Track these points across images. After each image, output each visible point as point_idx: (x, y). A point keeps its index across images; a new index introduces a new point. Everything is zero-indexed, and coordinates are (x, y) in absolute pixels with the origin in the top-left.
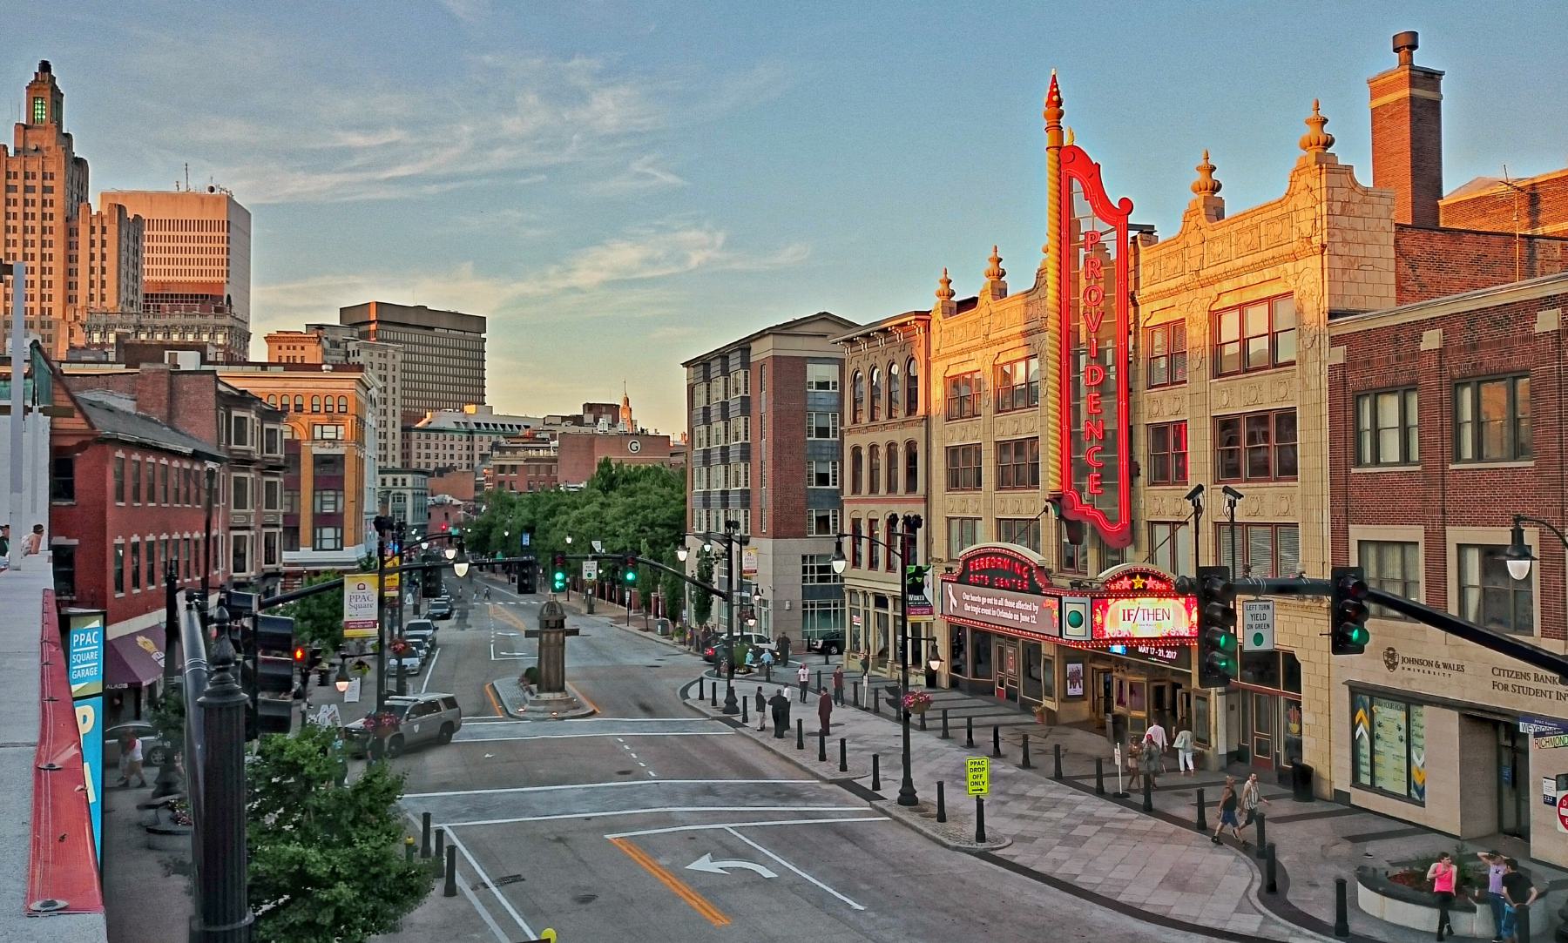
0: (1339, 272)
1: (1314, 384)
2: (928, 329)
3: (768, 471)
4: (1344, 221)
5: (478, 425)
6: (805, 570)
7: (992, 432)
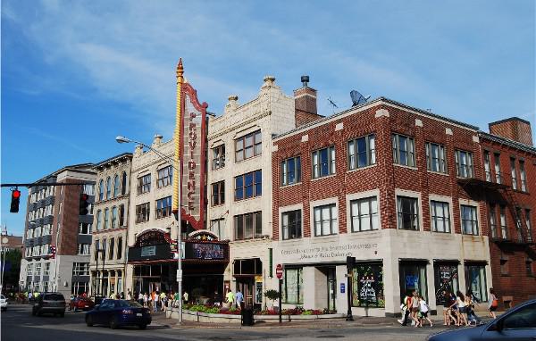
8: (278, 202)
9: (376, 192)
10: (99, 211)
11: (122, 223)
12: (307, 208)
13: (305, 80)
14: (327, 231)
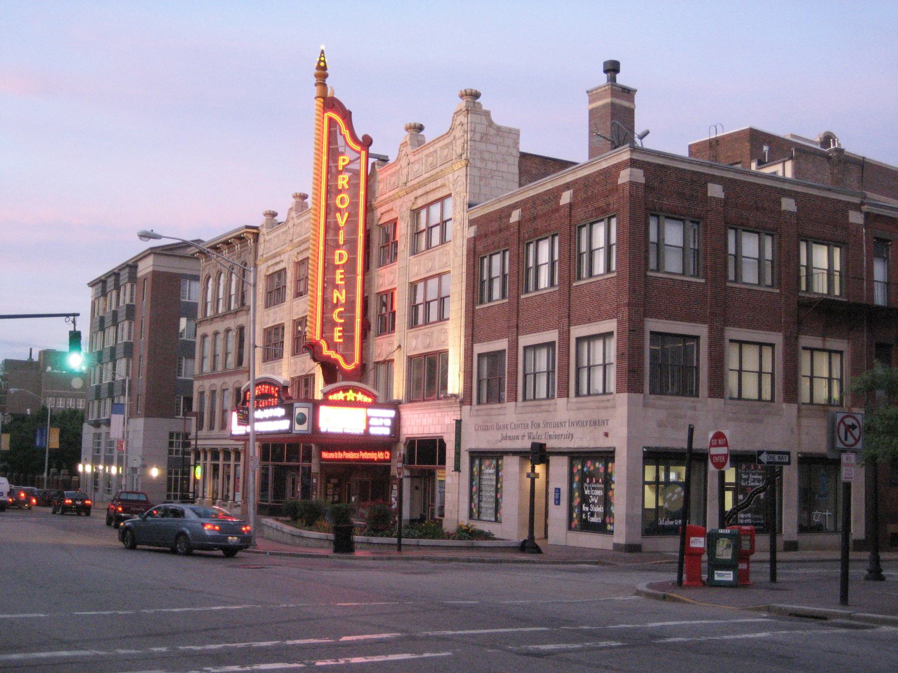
0: (477, 179)
3: (145, 362)
4: (482, 146)
6: (171, 444)
8: (472, 335)
9: (610, 325)
10: (204, 336)
11: (240, 361)
12: (514, 345)
13: (612, 68)
14: (598, 386)
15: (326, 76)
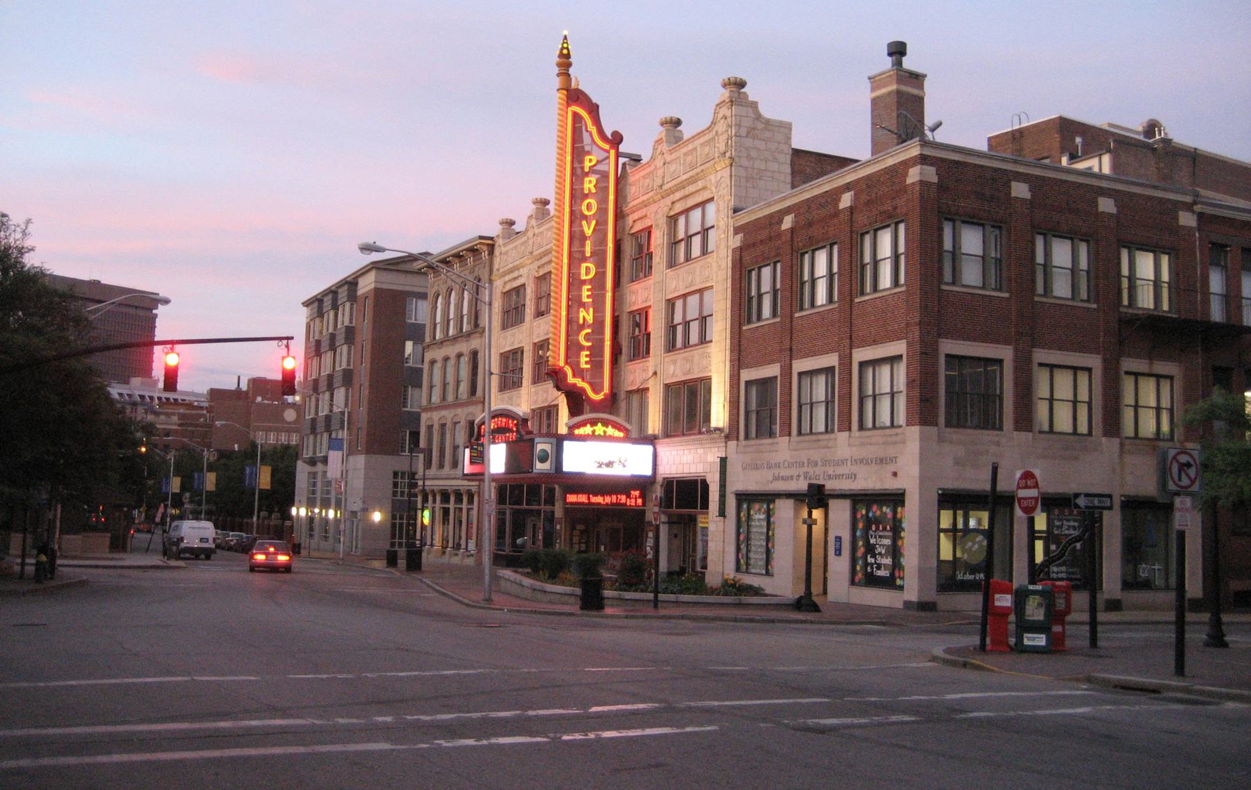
1: (724, 265)
2: (491, 253)
3: (365, 392)
4: (749, 142)
5: (142, 397)
7: (531, 333)
8: (740, 357)
9: (899, 347)
10: (433, 362)
11: (473, 390)
12: (787, 371)
13: (898, 50)
14: (885, 418)
15: (570, 65)
